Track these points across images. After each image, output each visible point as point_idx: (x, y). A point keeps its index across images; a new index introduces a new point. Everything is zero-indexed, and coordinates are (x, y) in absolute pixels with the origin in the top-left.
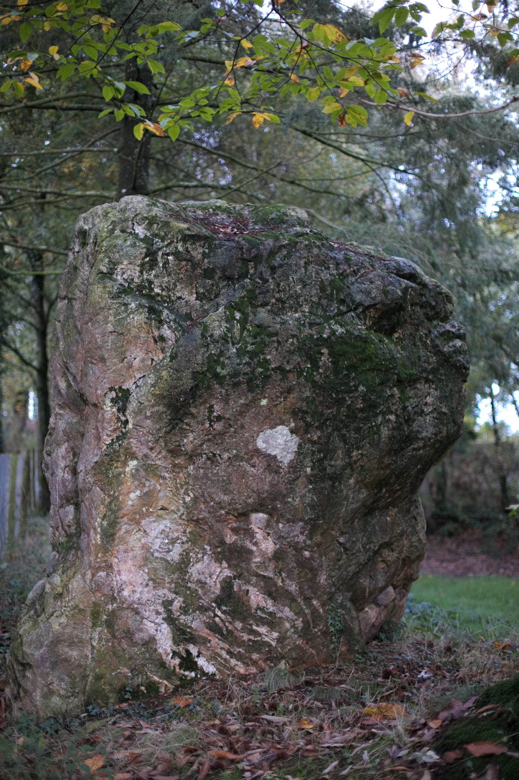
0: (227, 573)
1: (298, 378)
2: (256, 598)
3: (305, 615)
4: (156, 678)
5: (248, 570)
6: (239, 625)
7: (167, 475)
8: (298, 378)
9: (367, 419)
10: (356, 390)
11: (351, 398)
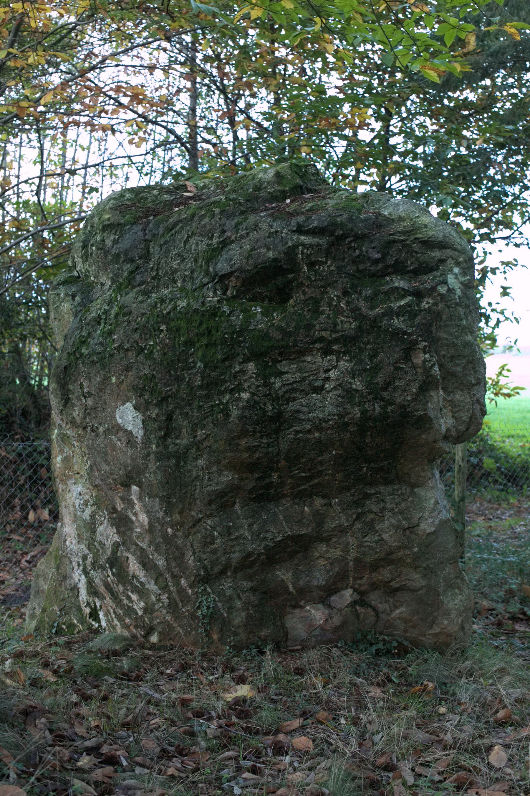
0: (116, 538)
1: (137, 356)
2: (134, 566)
3: (170, 593)
4: (75, 621)
5: (130, 538)
6: (121, 588)
7: (76, 444)
8: (137, 356)
9: (208, 397)
10: (194, 367)
11: (190, 374)
